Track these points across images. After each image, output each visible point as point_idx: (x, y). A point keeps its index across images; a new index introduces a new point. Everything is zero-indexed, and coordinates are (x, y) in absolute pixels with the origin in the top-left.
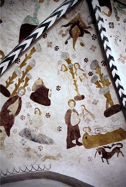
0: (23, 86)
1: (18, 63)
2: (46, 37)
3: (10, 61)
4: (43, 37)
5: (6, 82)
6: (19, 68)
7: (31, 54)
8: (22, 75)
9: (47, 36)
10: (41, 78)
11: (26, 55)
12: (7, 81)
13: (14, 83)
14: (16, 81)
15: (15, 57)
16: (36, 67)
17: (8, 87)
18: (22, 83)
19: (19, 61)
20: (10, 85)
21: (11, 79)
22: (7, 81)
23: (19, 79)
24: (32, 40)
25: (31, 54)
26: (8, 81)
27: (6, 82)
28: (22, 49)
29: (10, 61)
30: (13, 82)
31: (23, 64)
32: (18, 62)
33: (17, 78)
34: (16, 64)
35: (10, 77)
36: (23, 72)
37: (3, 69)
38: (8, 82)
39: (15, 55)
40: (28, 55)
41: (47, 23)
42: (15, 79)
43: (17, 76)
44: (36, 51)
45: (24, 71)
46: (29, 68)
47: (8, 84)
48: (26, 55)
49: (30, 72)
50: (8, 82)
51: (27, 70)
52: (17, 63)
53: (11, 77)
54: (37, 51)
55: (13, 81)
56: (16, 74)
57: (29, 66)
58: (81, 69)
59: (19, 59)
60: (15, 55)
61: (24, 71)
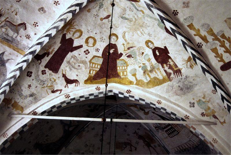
0: (229, 44)
1: (202, 45)
2: (176, 11)
3: (196, 59)
4: (177, 15)
5: (219, 62)
6: (208, 44)
7: (194, 29)
8: (217, 42)
9: (175, 10)
10: (225, 19)
11: (195, 35)
12: (218, 60)
13: (223, 53)
14: (221, 50)
15: (193, 53)
16: (211, 24)
17: (224, 61)
18: (226, 43)
19: (201, 43)
20: (223, 58)
21: (218, 55)
22: (218, 60)
23: (220, 46)
24: (178, 33)
25: (194, 29)
26: (219, 59)
27: (219, 61)
28: (186, 45)
29: (197, 58)
30: (221, 54)
31: (204, 39)
32: (201, 45)
33: (218, 48)
34: (204, 47)
35: (215, 56)
36: (213, 40)
37: (203, 66)
38: (220, 60)
39: (191, 53)
40: (194, 33)
41: (160, 18)
42: (218, 51)
43: (216, 48)
44: (192, 23)
45: (213, 39)
46: (211, 32)
47: (222, 60)
48: (195, 35)
49: (215, 32)
50: (220, 60)
51: (213, 34)
52: (202, 46)
53: (215, 55)
54: (192, 22)
55: (220, 54)
56: (214, 48)
57: (208, 32)
58: (135, 147)
59: (199, 43)
60: (191, 53)
61: (213, 39)
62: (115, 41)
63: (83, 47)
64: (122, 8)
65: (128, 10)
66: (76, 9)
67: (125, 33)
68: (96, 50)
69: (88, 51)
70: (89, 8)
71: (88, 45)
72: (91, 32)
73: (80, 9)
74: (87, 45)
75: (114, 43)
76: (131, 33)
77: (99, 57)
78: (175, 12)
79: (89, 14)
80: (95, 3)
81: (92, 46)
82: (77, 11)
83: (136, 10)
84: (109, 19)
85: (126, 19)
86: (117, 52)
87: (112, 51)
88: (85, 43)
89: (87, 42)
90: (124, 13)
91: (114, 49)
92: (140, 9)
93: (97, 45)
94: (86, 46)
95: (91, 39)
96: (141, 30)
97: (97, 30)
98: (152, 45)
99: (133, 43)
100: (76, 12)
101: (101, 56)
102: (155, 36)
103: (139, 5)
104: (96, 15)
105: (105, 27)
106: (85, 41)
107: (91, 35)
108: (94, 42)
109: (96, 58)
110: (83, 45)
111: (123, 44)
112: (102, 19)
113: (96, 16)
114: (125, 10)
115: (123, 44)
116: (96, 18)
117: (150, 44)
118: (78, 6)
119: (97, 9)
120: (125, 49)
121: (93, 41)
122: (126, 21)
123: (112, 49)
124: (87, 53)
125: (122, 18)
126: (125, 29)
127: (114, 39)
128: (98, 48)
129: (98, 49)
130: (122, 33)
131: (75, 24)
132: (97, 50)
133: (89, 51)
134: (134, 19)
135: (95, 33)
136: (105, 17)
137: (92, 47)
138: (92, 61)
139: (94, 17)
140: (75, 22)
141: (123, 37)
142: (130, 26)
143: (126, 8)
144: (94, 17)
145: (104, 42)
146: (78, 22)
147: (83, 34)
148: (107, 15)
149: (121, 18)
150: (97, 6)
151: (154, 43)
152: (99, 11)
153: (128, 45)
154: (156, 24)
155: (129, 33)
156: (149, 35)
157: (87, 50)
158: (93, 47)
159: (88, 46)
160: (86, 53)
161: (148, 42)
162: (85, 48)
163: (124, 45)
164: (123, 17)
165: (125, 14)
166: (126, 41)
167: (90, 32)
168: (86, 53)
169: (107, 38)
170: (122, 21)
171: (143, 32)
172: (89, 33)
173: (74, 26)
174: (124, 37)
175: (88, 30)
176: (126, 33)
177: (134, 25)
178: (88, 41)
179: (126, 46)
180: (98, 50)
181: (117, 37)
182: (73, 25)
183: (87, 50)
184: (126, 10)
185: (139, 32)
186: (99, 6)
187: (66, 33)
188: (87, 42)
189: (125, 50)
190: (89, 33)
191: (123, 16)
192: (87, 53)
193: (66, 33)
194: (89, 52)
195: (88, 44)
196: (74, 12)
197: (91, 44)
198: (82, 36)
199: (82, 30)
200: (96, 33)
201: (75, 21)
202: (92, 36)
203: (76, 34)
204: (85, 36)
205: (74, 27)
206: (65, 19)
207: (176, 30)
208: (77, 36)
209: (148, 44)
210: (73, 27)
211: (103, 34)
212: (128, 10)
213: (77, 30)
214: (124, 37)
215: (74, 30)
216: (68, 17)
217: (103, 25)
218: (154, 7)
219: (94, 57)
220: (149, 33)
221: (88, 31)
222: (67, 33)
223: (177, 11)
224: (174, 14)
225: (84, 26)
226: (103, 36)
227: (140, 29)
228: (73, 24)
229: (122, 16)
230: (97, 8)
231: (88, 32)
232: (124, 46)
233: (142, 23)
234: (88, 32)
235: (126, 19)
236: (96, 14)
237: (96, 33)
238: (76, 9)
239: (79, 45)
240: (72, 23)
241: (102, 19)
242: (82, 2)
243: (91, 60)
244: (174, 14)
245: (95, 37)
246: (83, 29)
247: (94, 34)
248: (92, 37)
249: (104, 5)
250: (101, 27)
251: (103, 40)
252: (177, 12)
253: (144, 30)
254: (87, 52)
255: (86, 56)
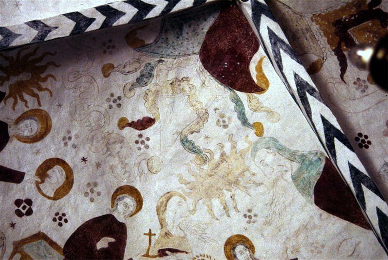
2: (366, 137)
4: (367, 147)
24: (370, 187)
62: (128, 213)
63: (22, 183)
64: (197, 110)
65: (213, 118)
66: (95, 19)
67: (169, 196)
68: (57, 217)
69: (28, 207)
70: (111, 62)
71: (41, 186)
72: (74, 146)
73: (105, 24)
74: (37, 184)
75: (120, 218)
76: (190, 201)
77: (53, 244)
78: (361, 139)
79: (100, 80)
80: (137, 54)
81: (52, 195)
82: (94, 27)
83: (239, 123)
84: (142, 132)
85: (193, 149)
86: (118, 250)
87: (102, 244)
88: (34, 172)
89: (43, 172)
90: (196, 128)
91: (112, 240)
92: (252, 118)
93: (67, 204)
94: (33, 185)
95: (60, 168)
96: (228, 195)
97: (93, 149)
98: (247, 252)
99: (184, 238)
100: (89, 29)
101: (61, 243)
102: (268, 223)
103: (258, 102)
104: (116, 97)
105: (118, 152)
106: (40, 166)
107: (65, 155)
108: (63, 187)
109: (44, 243)
110: (26, 178)
111: (150, 234)
112: (123, 124)
113: (114, 101)
114: (203, 117)
115: (150, 234)
116: (111, 107)
117: (240, 248)
118: (103, 13)
119: (130, 81)
120: (149, 249)
121: (64, 179)
122: (192, 156)
123: (109, 235)
124: (24, 211)
125: (184, 141)
126: (174, 185)
127: (126, 206)
128: (65, 212)
129: (64, 215)
130: (162, 194)
131: (48, 84)
132: (60, 219)
133: (34, 209)
134: (217, 157)
135: (82, 154)
136: (136, 120)
137: (49, 198)
138: (24, 247)
139: (108, 100)
140: (52, 76)
141: (157, 210)
142: (193, 179)
143: (211, 111)
144: (108, 100)
145: (92, 200)
146: (58, 84)
147: (48, 139)
148: (144, 118)
149: (182, 141)
150: (136, 70)
151: (256, 249)
152: (130, 90)
153: (164, 240)
154: (288, 176)
155: (183, 201)
156: (249, 216)
157: (29, 202)
158: (51, 201)
159: (39, 189)
160: (20, 208)
161: (234, 242)
162: (26, 189)
163: (153, 237)
164: (187, 141)
165: (198, 132)
166: (162, 225)
167: (70, 143)
168: (20, 208)
169: (109, 193)
170: (177, 154)
171: (230, 204)
172: (66, 144)
173: (40, 89)
174: (162, 209)
175: (69, 132)
176: (174, 200)
177: (210, 176)
178: (49, 172)
179: (158, 242)
180: (62, 221)
181: (139, 203)
182: (41, 84)
183: (29, 202)
184: (206, 119)
185: (216, 203)
186: (139, 75)
187: (7, 93)
188: (43, 172)
189: (151, 253)
190: (66, 144)
191: (190, 137)
192: (24, 211)
193: (7, 93)
194: (30, 212)
195: (43, 182)
196: (82, 24)
197: (49, 188)
198: (40, 142)
199: (54, 121)
200: (84, 160)
201: (53, 73)
202: (68, 160)
203: (28, 122)
204: (49, 148)
205: (41, 94)
206: (46, 26)
207: (367, 175)
208: (26, 133)
209: (234, 248)
210: (36, 91)
211: (103, 175)
212: (213, 118)
213: (41, 111)
214: (161, 209)
215: (32, 104)
216: (57, 28)
217: (118, 146)
218: (317, 94)
219: (40, 236)
220: (249, 211)
221: (67, 140)
222: (9, 96)
223: (368, 139)
224: (360, 142)
225: (64, 112)
226: (98, 180)
227: (225, 191)
228: (45, 80)
229: (186, 137)
230: (132, 78)
231: (64, 139)
232: (150, 240)
233: (240, 170)
234: (66, 139)
235: (193, 149)
236: (118, 93)
237: (84, 160)
238: (95, 19)
239: (15, 167)
240: (43, 76)
241: (123, 124)
242: (120, 10)
243: (24, 241)
244: (360, 142)
245: (75, 171)
246: (59, 119)
247: (78, 160)
248: (68, 165)
249: (155, 77)
250: (108, 149)
251: (94, 196)
252: (366, 140)
253: (236, 197)
254: (24, 208)
255: (16, 219)
